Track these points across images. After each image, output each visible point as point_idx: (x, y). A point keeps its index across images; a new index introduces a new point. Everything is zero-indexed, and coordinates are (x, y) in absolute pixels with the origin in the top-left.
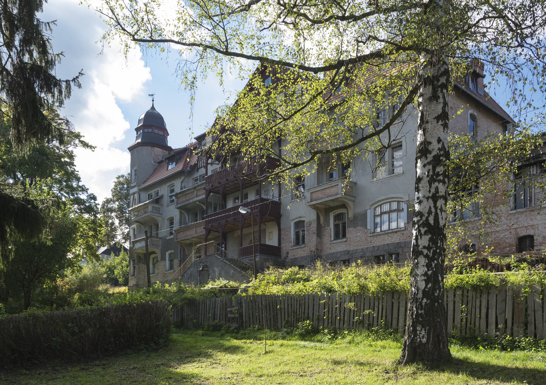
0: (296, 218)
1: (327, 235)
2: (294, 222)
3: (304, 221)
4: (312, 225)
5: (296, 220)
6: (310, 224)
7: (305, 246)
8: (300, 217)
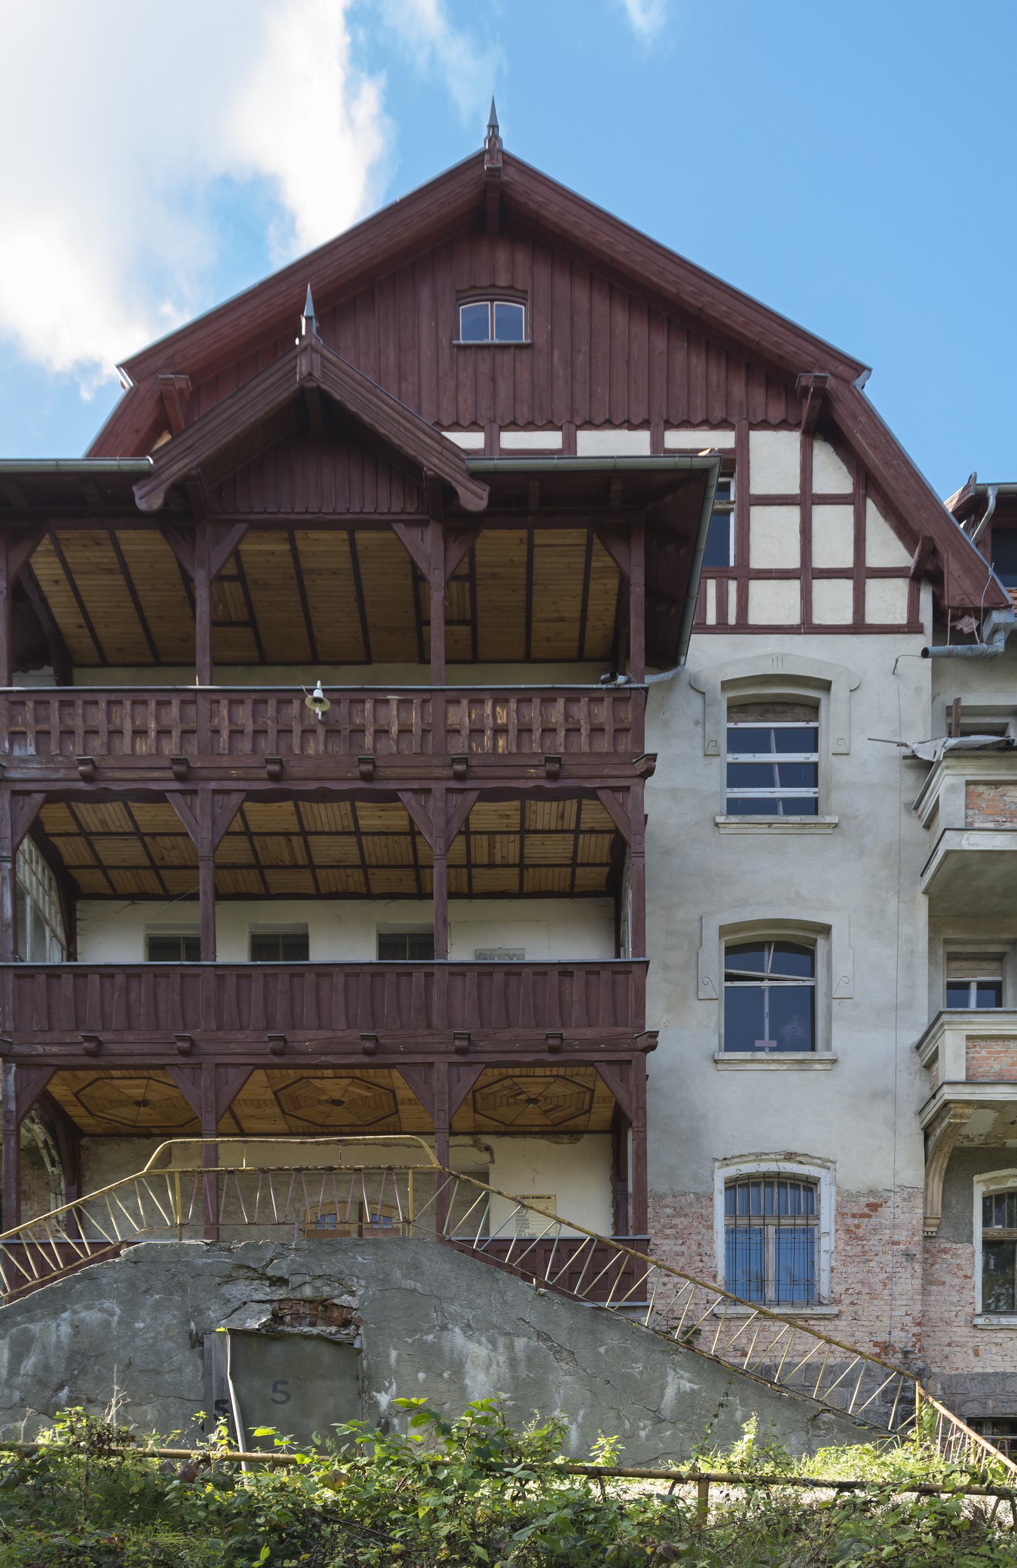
0: (759, 1157)
1: (948, 1279)
2: (732, 1171)
3: (810, 1185)
4: (886, 1212)
5: (749, 1168)
6: (874, 1207)
7: (837, 1316)
8: (790, 1156)
